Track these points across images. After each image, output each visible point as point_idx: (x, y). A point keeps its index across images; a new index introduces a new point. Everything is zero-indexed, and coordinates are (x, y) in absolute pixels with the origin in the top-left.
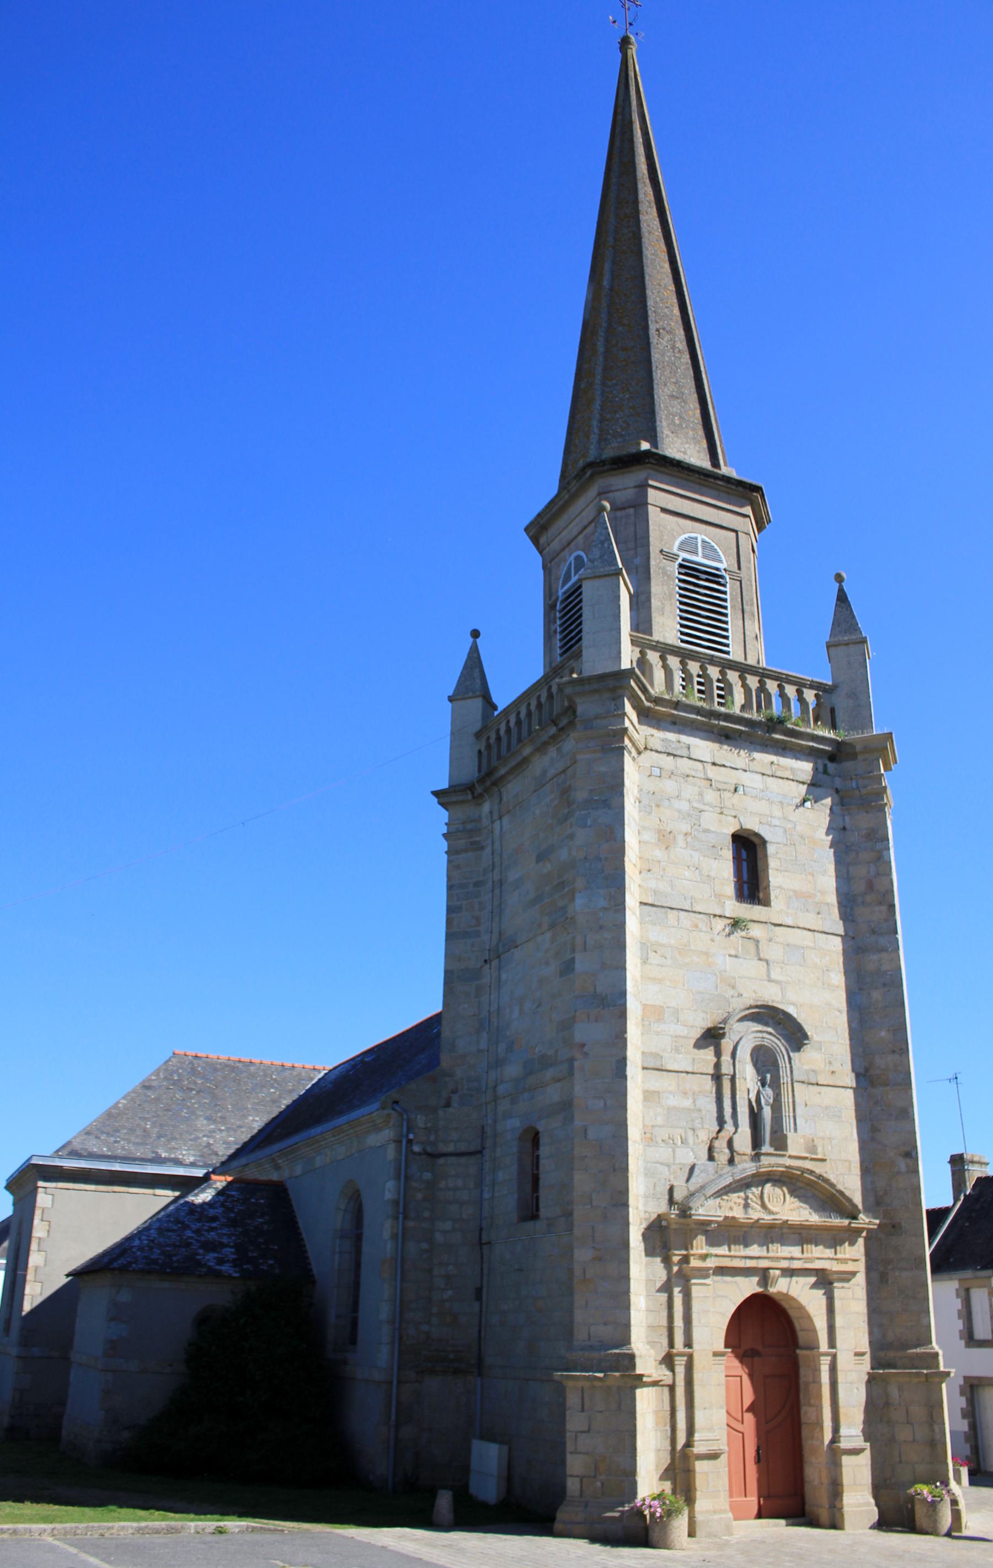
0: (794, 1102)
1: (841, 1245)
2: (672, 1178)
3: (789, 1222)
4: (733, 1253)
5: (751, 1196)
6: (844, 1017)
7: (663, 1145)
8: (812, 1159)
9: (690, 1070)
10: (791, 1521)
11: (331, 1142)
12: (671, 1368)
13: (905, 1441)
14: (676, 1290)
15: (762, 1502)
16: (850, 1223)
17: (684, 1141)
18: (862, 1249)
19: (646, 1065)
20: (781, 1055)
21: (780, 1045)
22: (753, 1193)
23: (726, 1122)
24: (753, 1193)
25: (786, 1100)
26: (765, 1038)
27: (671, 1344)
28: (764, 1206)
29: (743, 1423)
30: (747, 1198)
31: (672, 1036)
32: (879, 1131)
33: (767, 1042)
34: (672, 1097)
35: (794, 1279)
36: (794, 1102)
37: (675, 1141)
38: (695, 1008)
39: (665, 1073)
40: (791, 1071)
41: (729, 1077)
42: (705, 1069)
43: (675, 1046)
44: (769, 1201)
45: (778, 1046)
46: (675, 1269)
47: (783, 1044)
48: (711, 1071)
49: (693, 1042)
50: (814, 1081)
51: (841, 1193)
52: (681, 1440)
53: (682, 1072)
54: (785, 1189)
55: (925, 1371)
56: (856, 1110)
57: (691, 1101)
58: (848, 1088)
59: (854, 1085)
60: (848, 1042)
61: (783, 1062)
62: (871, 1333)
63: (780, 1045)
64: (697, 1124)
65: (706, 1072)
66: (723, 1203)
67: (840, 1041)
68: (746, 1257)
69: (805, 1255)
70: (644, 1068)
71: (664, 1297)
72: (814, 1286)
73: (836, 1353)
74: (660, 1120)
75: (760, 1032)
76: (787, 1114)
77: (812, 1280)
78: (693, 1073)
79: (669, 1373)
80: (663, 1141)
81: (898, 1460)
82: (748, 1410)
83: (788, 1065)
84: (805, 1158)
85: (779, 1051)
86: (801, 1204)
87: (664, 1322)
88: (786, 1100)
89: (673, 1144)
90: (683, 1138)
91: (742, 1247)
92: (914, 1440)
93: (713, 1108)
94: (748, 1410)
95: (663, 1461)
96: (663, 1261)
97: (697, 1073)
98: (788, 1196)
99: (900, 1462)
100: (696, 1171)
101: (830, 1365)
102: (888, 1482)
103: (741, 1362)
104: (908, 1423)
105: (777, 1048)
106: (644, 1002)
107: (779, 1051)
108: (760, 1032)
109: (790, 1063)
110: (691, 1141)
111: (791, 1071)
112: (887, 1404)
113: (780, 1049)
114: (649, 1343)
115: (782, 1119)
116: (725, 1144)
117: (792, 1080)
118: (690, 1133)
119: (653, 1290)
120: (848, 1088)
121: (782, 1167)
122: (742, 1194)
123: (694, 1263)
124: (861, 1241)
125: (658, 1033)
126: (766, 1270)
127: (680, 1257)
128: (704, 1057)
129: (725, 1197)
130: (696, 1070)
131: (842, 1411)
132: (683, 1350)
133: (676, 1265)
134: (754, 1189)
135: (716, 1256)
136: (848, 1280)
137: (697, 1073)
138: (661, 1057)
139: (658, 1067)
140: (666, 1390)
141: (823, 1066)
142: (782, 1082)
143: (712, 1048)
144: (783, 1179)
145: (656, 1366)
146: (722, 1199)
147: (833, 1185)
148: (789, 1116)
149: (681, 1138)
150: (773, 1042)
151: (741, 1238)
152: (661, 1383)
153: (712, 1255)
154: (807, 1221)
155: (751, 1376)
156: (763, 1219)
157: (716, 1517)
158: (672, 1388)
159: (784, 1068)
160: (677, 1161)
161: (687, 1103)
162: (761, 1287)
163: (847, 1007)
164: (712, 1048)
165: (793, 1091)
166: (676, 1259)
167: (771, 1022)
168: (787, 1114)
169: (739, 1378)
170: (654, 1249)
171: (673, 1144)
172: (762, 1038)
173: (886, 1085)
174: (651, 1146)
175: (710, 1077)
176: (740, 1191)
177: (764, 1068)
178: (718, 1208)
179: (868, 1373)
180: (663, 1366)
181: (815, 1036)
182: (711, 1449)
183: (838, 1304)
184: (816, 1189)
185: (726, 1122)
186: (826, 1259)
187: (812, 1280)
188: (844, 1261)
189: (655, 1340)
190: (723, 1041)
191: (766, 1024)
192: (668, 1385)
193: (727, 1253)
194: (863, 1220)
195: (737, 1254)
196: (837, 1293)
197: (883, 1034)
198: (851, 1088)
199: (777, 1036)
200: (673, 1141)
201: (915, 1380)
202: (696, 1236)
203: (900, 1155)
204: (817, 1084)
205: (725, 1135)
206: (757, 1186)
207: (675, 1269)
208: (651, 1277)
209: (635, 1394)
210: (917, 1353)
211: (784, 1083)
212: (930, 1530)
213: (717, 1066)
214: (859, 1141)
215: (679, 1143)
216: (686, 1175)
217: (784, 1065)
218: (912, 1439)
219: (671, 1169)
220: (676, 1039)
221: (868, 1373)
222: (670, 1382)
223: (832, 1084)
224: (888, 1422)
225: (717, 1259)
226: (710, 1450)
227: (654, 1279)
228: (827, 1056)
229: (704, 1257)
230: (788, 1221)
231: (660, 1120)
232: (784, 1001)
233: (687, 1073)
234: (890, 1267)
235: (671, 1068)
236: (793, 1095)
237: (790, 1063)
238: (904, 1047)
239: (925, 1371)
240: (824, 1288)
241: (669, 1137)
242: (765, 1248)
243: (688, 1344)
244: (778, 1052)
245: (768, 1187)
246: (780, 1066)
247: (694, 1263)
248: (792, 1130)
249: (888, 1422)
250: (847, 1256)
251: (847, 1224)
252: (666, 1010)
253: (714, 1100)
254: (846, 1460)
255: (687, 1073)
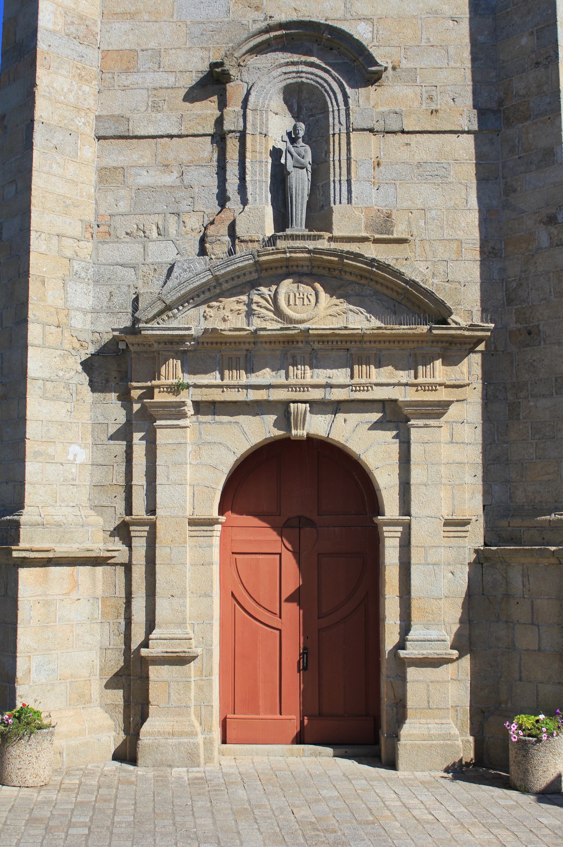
0: (349, 159)
1: (425, 364)
2: (140, 283)
3: (311, 332)
4: (226, 381)
5: (256, 298)
6: (464, 27)
7: (128, 239)
8: (376, 241)
9: (175, 132)
10: (342, 751)
11: (403, 329)
12: (128, 541)
13: (528, 650)
14: (137, 436)
15: (306, 721)
16: (430, 330)
17: (162, 232)
18: (478, 371)
19: (101, 134)
20: (331, 94)
21: (330, 79)
22: (261, 296)
23: (229, 199)
24: (261, 296)
25: (337, 158)
26: (302, 72)
27: (129, 510)
28: (278, 312)
29: (280, 617)
30: (249, 304)
31: (148, 90)
32: (515, 191)
33: (307, 78)
34: (145, 173)
35: (340, 416)
36: (349, 159)
37: (148, 233)
38: (188, 46)
39: (134, 141)
40: (348, 115)
41: (238, 134)
42: (200, 128)
43: (153, 102)
44: (289, 305)
45: (326, 81)
46: (136, 407)
47: (334, 78)
48: (211, 130)
49: (183, 92)
50: (396, 128)
51: (414, 284)
52: (138, 636)
53: (162, 137)
54: (317, 285)
55: (553, 548)
56: (478, 165)
57: (176, 174)
58: (463, 132)
59: (475, 127)
60: (468, 64)
61: (334, 103)
62: (487, 493)
63: (330, 79)
64: (184, 207)
65: (202, 132)
66: (211, 312)
67: (452, 64)
68: (247, 387)
69: (356, 380)
70: (99, 138)
71: (120, 446)
72: (376, 426)
73: (410, 520)
74: (123, 207)
75: (293, 64)
76: (337, 178)
77: (375, 416)
78: (180, 136)
79: (125, 548)
80: (127, 234)
81: (517, 676)
82: (288, 600)
83: (342, 107)
84: (364, 240)
85: (328, 89)
86: (351, 307)
87: (121, 480)
88: (337, 158)
89: (145, 236)
90: (161, 227)
91: (243, 372)
92: (539, 650)
93: (214, 181)
94: (288, 600)
95: (113, 663)
96: (119, 398)
97: (187, 136)
98: (323, 295)
99: (520, 679)
100: (176, 271)
101: (148, 538)
102: (503, 706)
103: (281, 535)
104: (532, 624)
105: (325, 85)
106: (104, 47)
107: (328, 89)
108: (293, 64)
109: (346, 104)
110: (172, 231)
111: (348, 115)
112: (507, 596)
113: (329, 85)
114: (94, 507)
115: (330, 186)
116: (224, 230)
117: (348, 128)
118: (172, 219)
119: (104, 437)
120: (463, 132)
121: (302, 252)
122: (244, 298)
123: (159, 397)
124: (475, 359)
125: (125, 88)
126: (286, 404)
127: (142, 391)
128: (200, 112)
129: (214, 304)
130: (184, 132)
131: (415, 604)
132: (145, 517)
133: (137, 402)
134: (264, 290)
135: (196, 386)
136: (439, 416)
137: (187, 136)
138: (128, 120)
139: (122, 134)
140: (120, 571)
141: (416, 104)
142: (331, 132)
143: (215, 98)
144: (315, 271)
145: (104, 539)
146: (209, 307)
147: (399, 275)
148: (340, 181)
149: (158, 228)
150: (317, 76)
151: (242, 360)
152: (112, 561)
153: (188, 386)
154: (346, 328)
155: (297, 554)
156: (264, 329)
157: (173, 741)
158: (128, 567)
159: (336, 113)
160: (149, 260)
161: (170, 179)
162: (279, 429)
163: (470, 12)
164: (215, 98)
165: (348, 144)
166: (135, 394)
167: (315, 47)
168: (337, 178)
169: (279, 555)
170: (107, 381)
171: (145, 236)
172: (297, 72)
173: (527, 119)
174: (107, 243)
175: (209, 139)
176: (242, 293)
177: (311, 118)
178: (202, 319)
179: (477, 551)
180: (117, 539)
181: (404, 61)
182: (169, 650)
183: (415, 450)
184: (377, 282)
185: (229, 199)
186: (394, 385)
187: (375, 416)
188: (433, 387)
189: (105, 504)
190: (230, 87)
191: (309, 53)
192: (122, 564)
193: (218, 381)
194: (456, 323)
195: (234, 382)
196: (415, 434)
197: (524, 41)
198: (468, 132)
199: (323, 65)
200: (144, 232)
201: (545, 561)
202: (166, 360)
203: (540, 222)
204: (403, 132)
205: (227, 217)
206: (268, 285)
207: (136, 407)
208: (101, 420)
209: (17, 573)
210: (550, 521)
211: (334, 134)
212: (518, 783)
213: (219, 122)
214: (480, 211)
215: (155, 234)
216: (163, 278)
217: (336, 108)
218: (537, 648)
219: (140, 273)
220: (155, 92)
221: (477, 551)
222: (125, 560)
223: (430, 129)
224: (507, 622)
225: (198, 391)
226: (167, 652)
227: (106, 421)
228: (424, 89)
229: (177, 389)
230: (309, 329)
231: (123, 207)
232: (348, 16)
233: (171, 137)
234: (522, 395)
235: (142, 133)
236: (349, 150)
237: (346, 104)
238: (552, 53)
239: (553, 548)
240: (397, 428)
241: (138, 229)
242: (283, 372)
243: (152, 510)
244: (326, 91)
245: (287, 286)
246: (331, 109)
247: (159, 397)
248: (344, 201)
249: (507, 622)
250: (438, 380)
251: (425, 331)
252: (140, 54)
253: (215, 170)
254: (412, 673)
255: (171, 137)
